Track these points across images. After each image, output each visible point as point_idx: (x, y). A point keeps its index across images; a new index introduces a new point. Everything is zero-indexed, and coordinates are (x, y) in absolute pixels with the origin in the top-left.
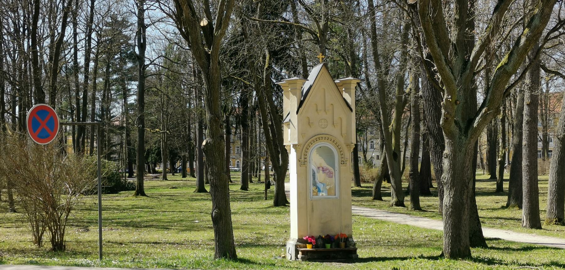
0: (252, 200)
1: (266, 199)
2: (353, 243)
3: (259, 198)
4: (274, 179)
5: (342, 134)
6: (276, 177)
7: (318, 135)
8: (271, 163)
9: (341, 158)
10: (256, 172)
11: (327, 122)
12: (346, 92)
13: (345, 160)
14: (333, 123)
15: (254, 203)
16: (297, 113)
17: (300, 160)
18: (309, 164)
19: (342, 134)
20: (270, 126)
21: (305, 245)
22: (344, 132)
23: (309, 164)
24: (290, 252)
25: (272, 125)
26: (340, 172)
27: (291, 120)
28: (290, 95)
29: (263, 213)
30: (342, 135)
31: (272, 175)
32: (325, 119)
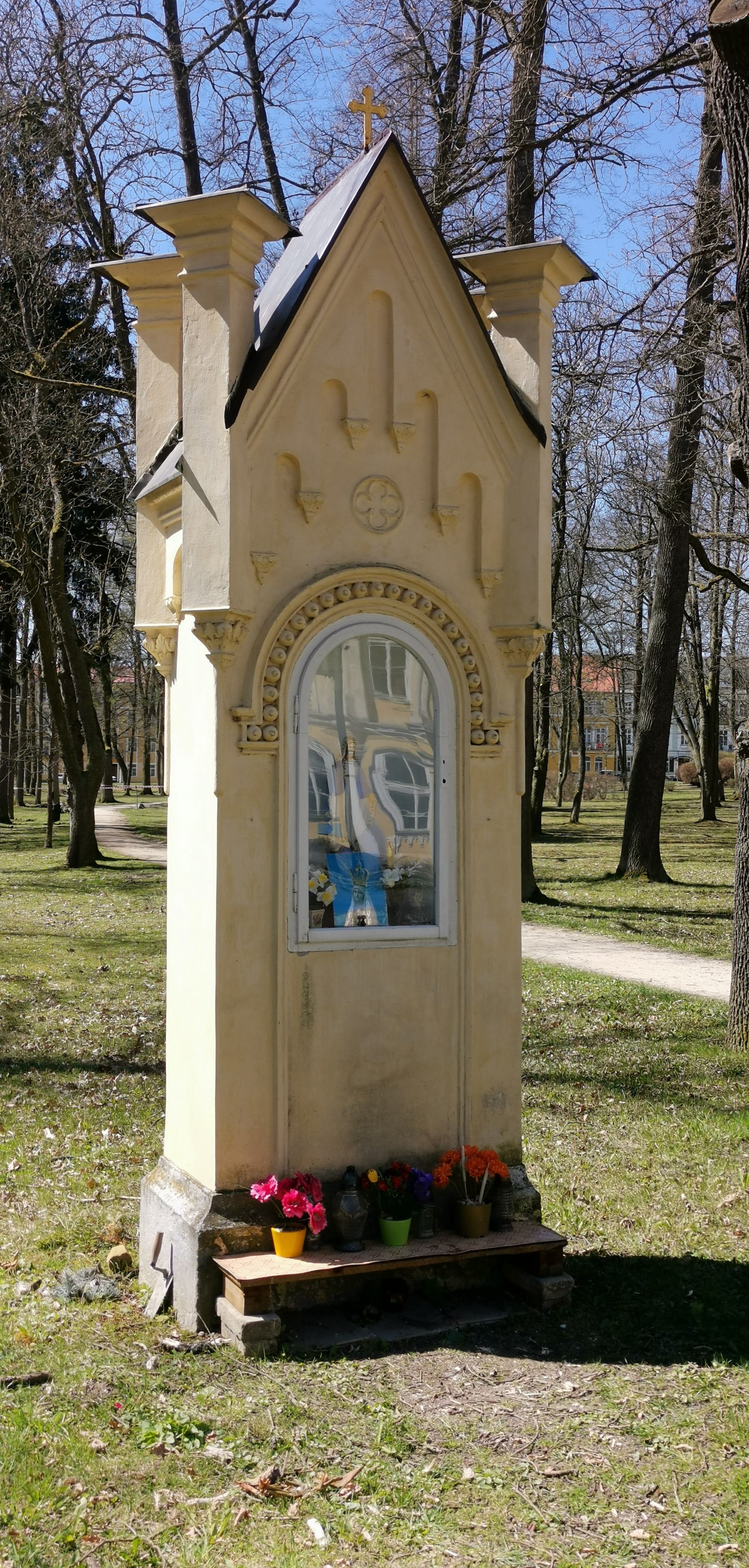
0: (18, 846)
1: (50, 846)
2: (530, 1194)
3: (37, 845)
4: (70, 801)
5: (477, 570)
6: (74, 797)
7: (344, 567)
8: (62, 765)
9: (473, 708)
10: (34, 786)
11: (400, 497)
12: (505, 332)
13: (495, 719)
14: (434, 506)
15: (21, 855)
16: (230, 417)
17: (240, 712)
18: (291, 736)
19: (477, 570)
20: (61, 676)
21: (258, 1230)
22: (491, 558)
23: (291, 736)
24: (163, 1262)
25: (67, 674)
26: (462, 791)
27: (190, 462)
28: (186, 305)
29: (37, 886)
30: (479, 580)
31: (64, 792)
32: (387, 481)
